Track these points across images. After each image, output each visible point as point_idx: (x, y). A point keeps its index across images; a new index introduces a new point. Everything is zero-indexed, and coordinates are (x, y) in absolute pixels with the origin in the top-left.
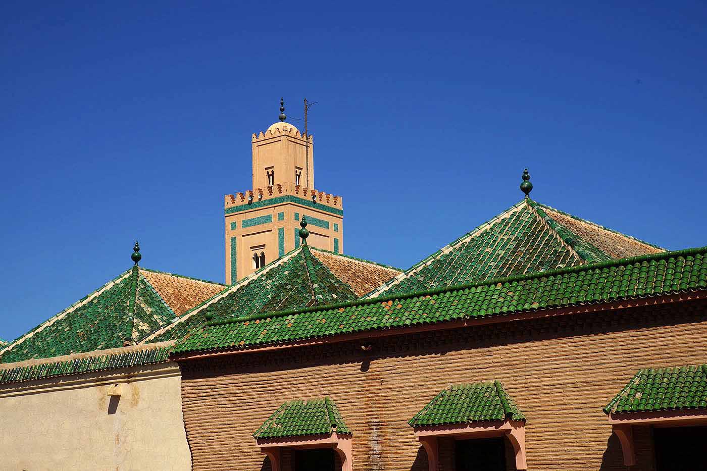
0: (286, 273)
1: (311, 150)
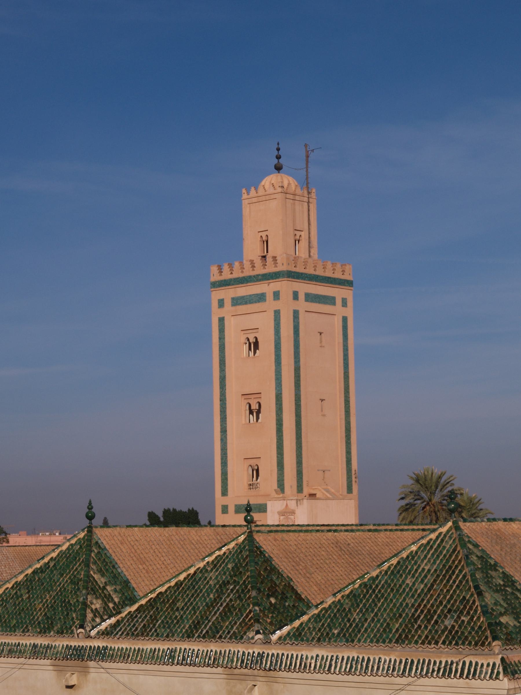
0: (230, 566)
1: (313, 201)
